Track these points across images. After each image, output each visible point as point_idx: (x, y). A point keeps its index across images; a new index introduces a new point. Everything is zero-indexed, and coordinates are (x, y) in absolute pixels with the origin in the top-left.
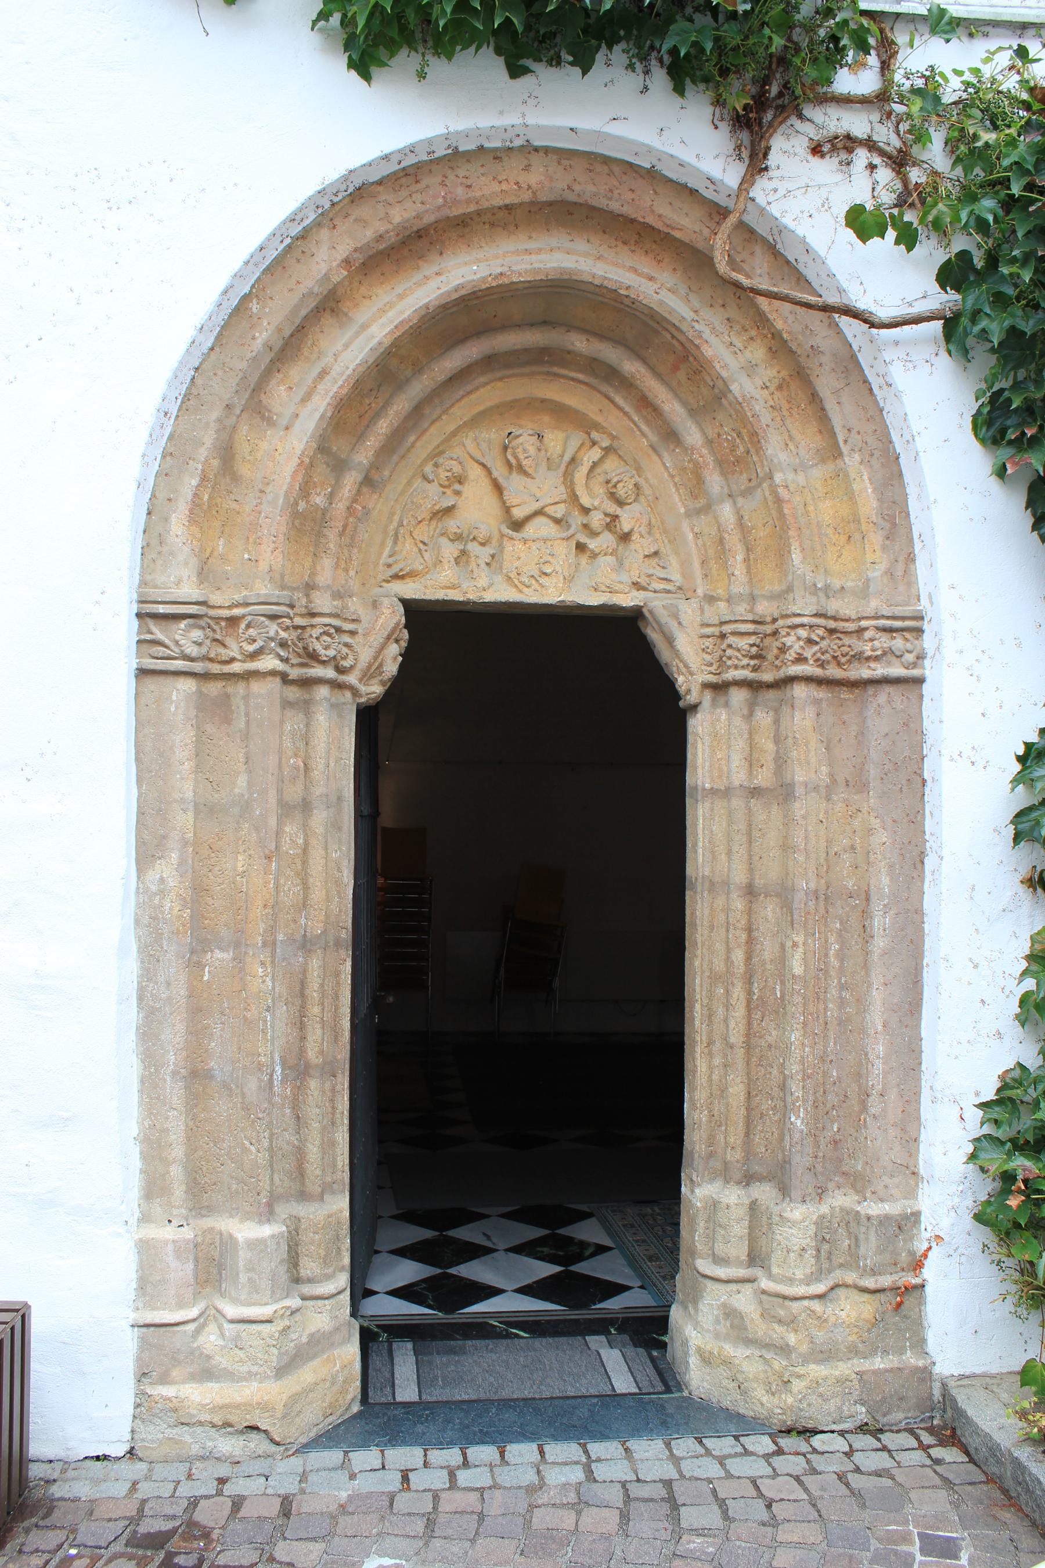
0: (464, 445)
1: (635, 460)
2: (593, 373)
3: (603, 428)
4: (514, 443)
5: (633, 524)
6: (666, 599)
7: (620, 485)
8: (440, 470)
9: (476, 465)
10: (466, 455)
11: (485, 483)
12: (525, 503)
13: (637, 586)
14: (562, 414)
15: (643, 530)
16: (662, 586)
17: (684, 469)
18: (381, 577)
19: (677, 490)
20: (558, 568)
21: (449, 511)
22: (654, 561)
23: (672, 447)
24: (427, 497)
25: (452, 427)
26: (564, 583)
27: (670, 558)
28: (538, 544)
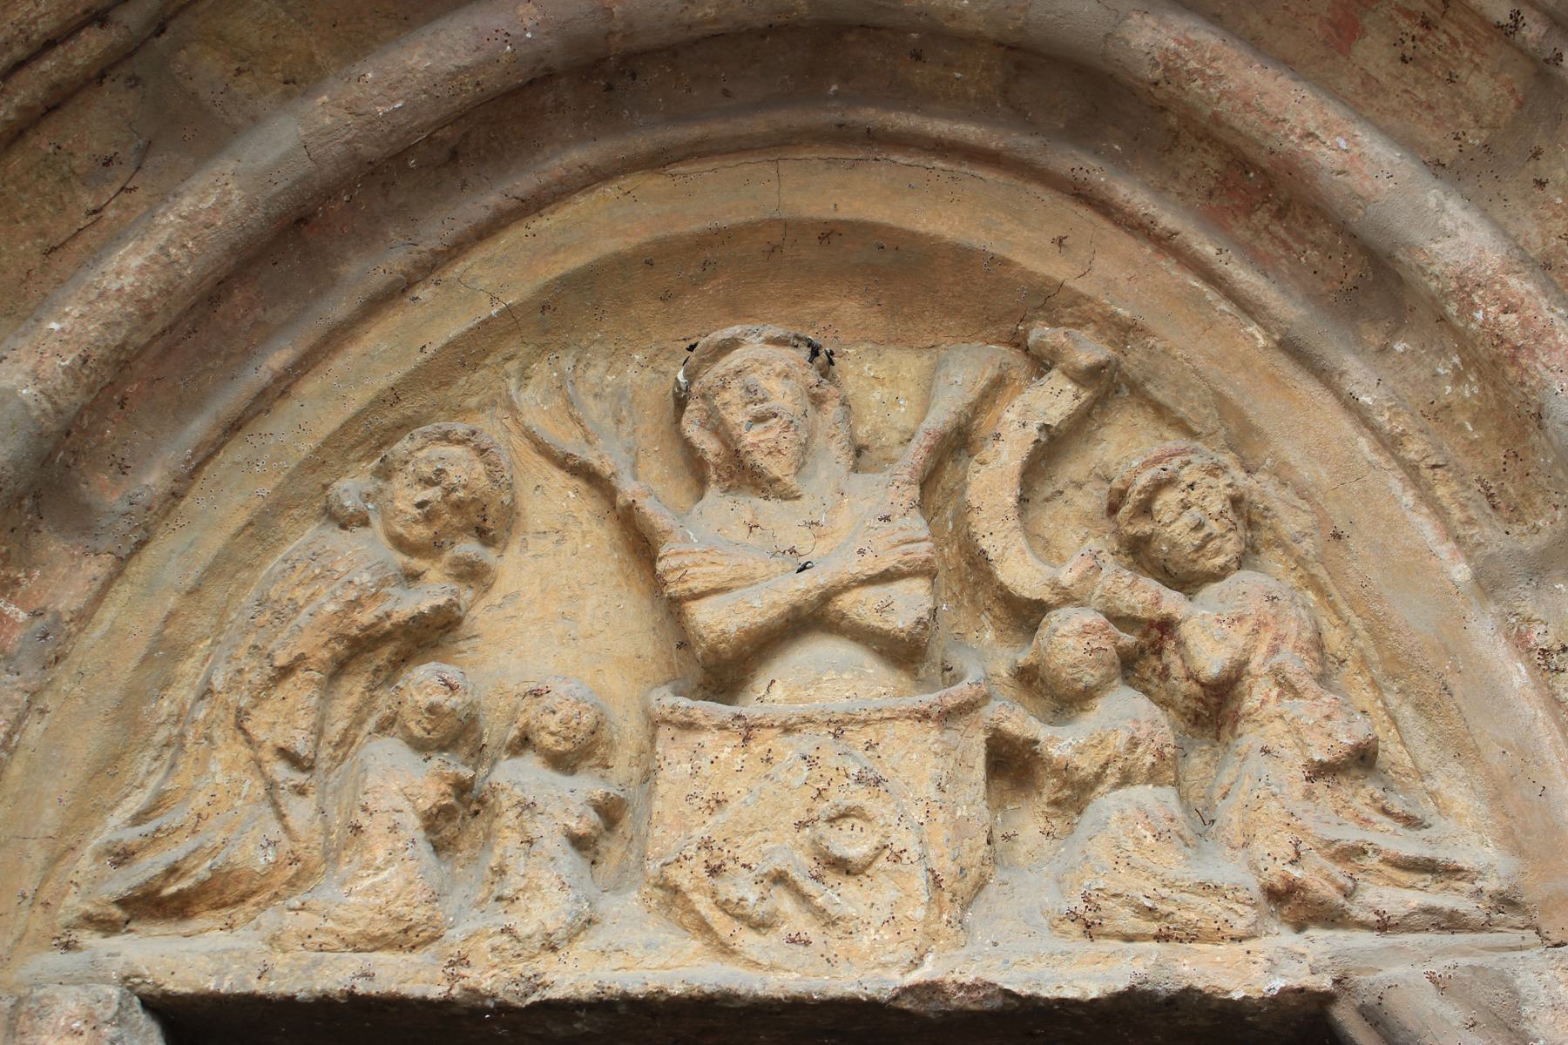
0: (512, 408)
1: (1221, 402)
2: (1006, 104)
3: (1077, 299)
4: (710, 377)
5: (1239, 636)
6: (1444, 952)
7: (1169, 500)
8: (399, 483)
9: (559, 477)
10: (518, 441)
11: (591, 542)
12: (751, 581)
13: (1287, 901)
14: (912, 282)
15: (1295, 665)
16: (1416, 899)
17: (1439, 413)
18: (75, 904)
19: (1426, 497)
20: (903, 839)
21: (432, 634)
22: (1361, 794)
23: (1375, 338)
24: (326, 574)
25: (456, 326)
26: (934, 903)
27: (1439, 783)
28: (804, 742)
